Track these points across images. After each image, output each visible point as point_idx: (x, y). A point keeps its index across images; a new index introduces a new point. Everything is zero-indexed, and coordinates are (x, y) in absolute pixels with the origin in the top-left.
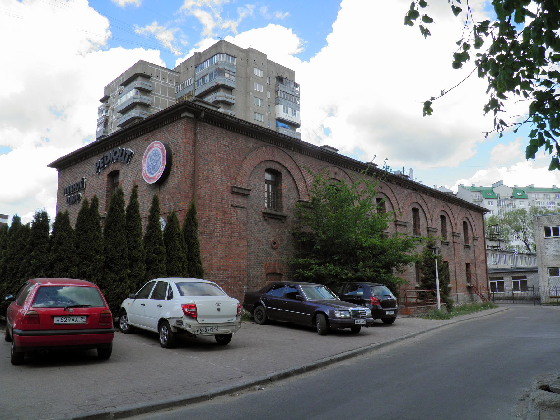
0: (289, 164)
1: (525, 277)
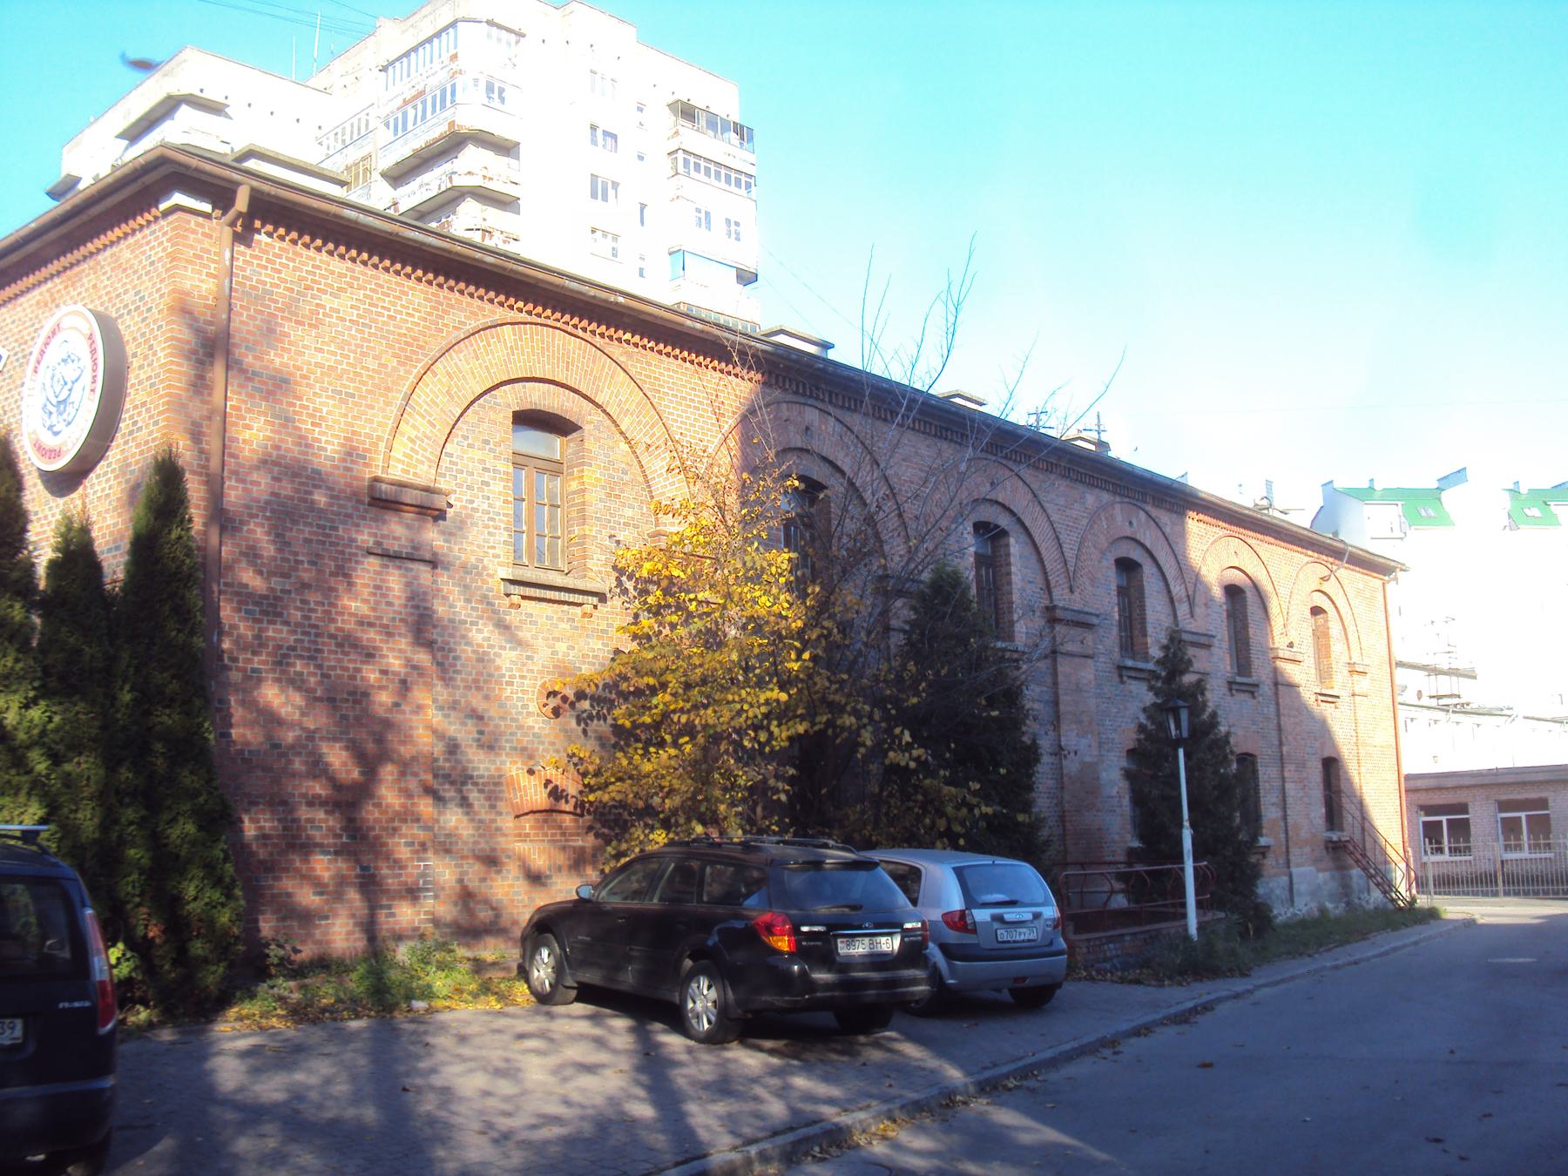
0: (1019, 500)
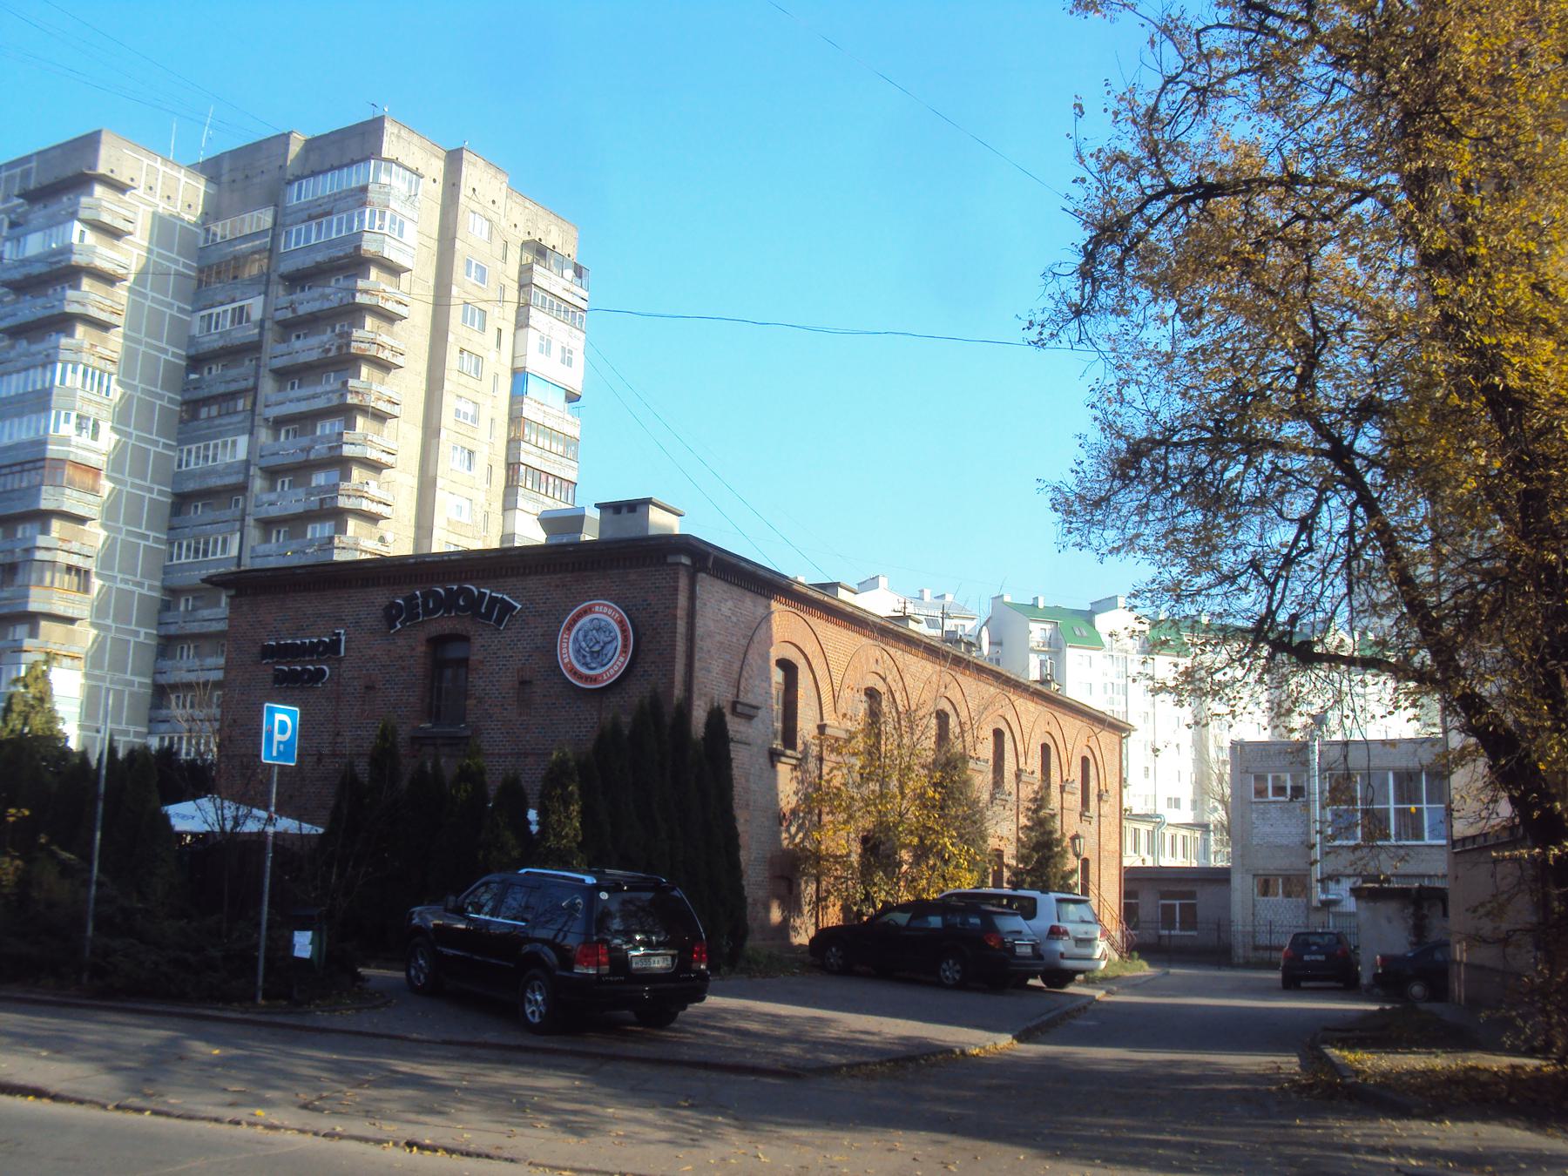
1: (1192, 895)
